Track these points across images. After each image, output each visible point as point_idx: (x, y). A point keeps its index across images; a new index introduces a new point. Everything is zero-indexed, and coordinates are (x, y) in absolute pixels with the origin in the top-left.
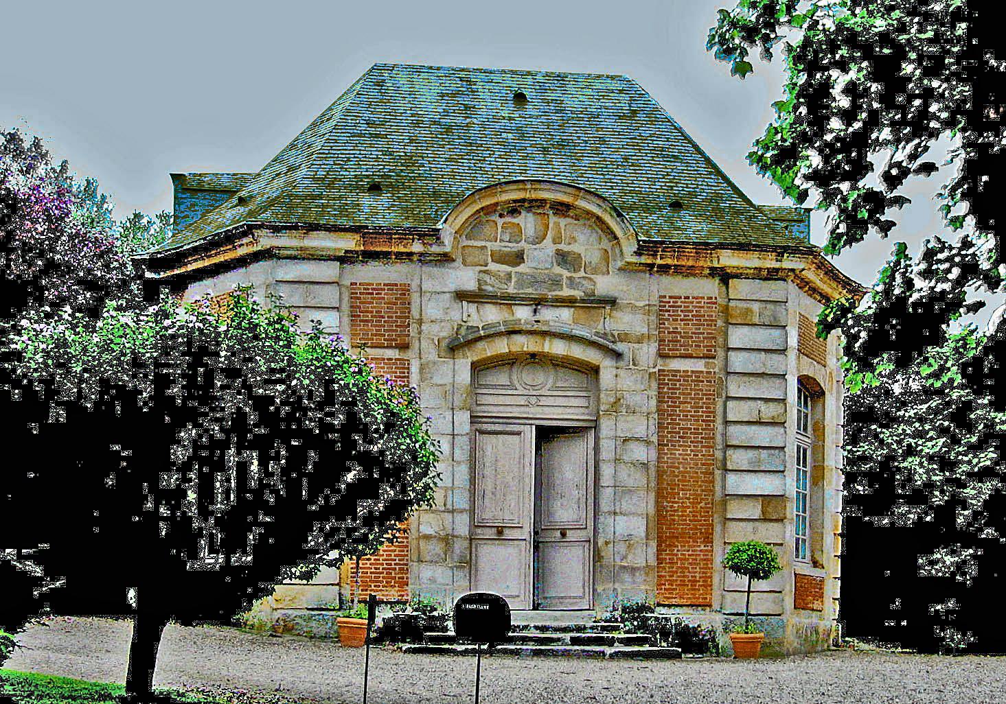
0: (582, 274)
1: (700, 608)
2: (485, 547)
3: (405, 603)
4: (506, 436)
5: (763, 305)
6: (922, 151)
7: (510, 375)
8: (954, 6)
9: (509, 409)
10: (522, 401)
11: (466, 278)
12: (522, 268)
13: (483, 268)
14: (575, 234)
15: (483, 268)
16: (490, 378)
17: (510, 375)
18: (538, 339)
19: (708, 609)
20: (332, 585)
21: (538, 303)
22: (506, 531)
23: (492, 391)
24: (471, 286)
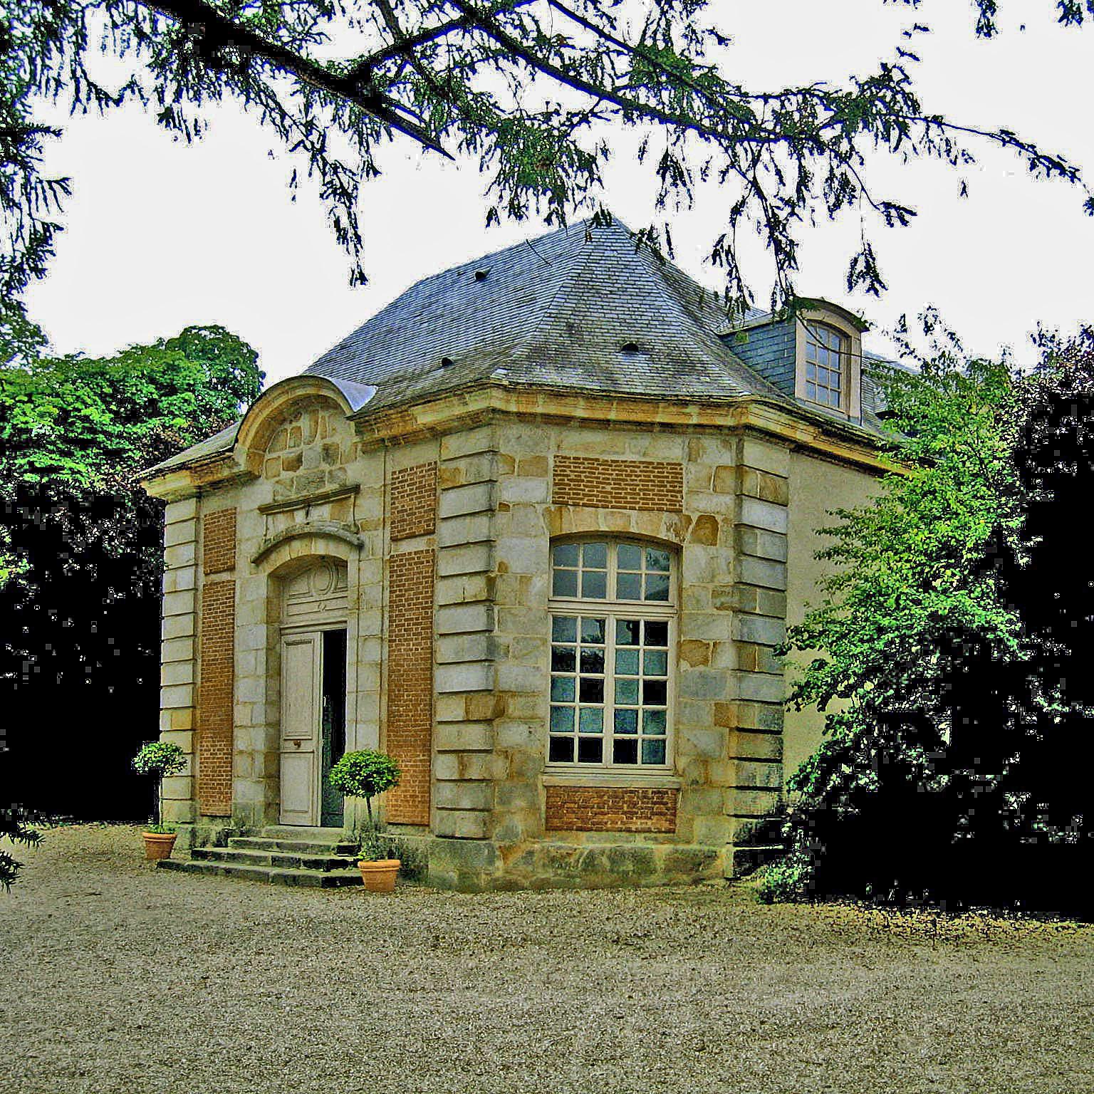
0: (338, 465)
1: (421, 828)
2: (290, 760)
3: (229, 817)
4: (304, 646)
5: (468, 460)
6: (273, 100)
7: (308, 584)
8: (860, 129)
9: (306, 617)
10: (315, 607)
11: (263, 492)
12: (301, 471)
13: (277, 479)
14: (335, 426)
15: (277, 479)
16: (297, 587)
17: (308, 584)
18: (306, 542)
19: (427, 829)
20: (294, 811)
21: (307, 504)
22: (303, 744)
23: (304, 600)
24: (268, 500)
